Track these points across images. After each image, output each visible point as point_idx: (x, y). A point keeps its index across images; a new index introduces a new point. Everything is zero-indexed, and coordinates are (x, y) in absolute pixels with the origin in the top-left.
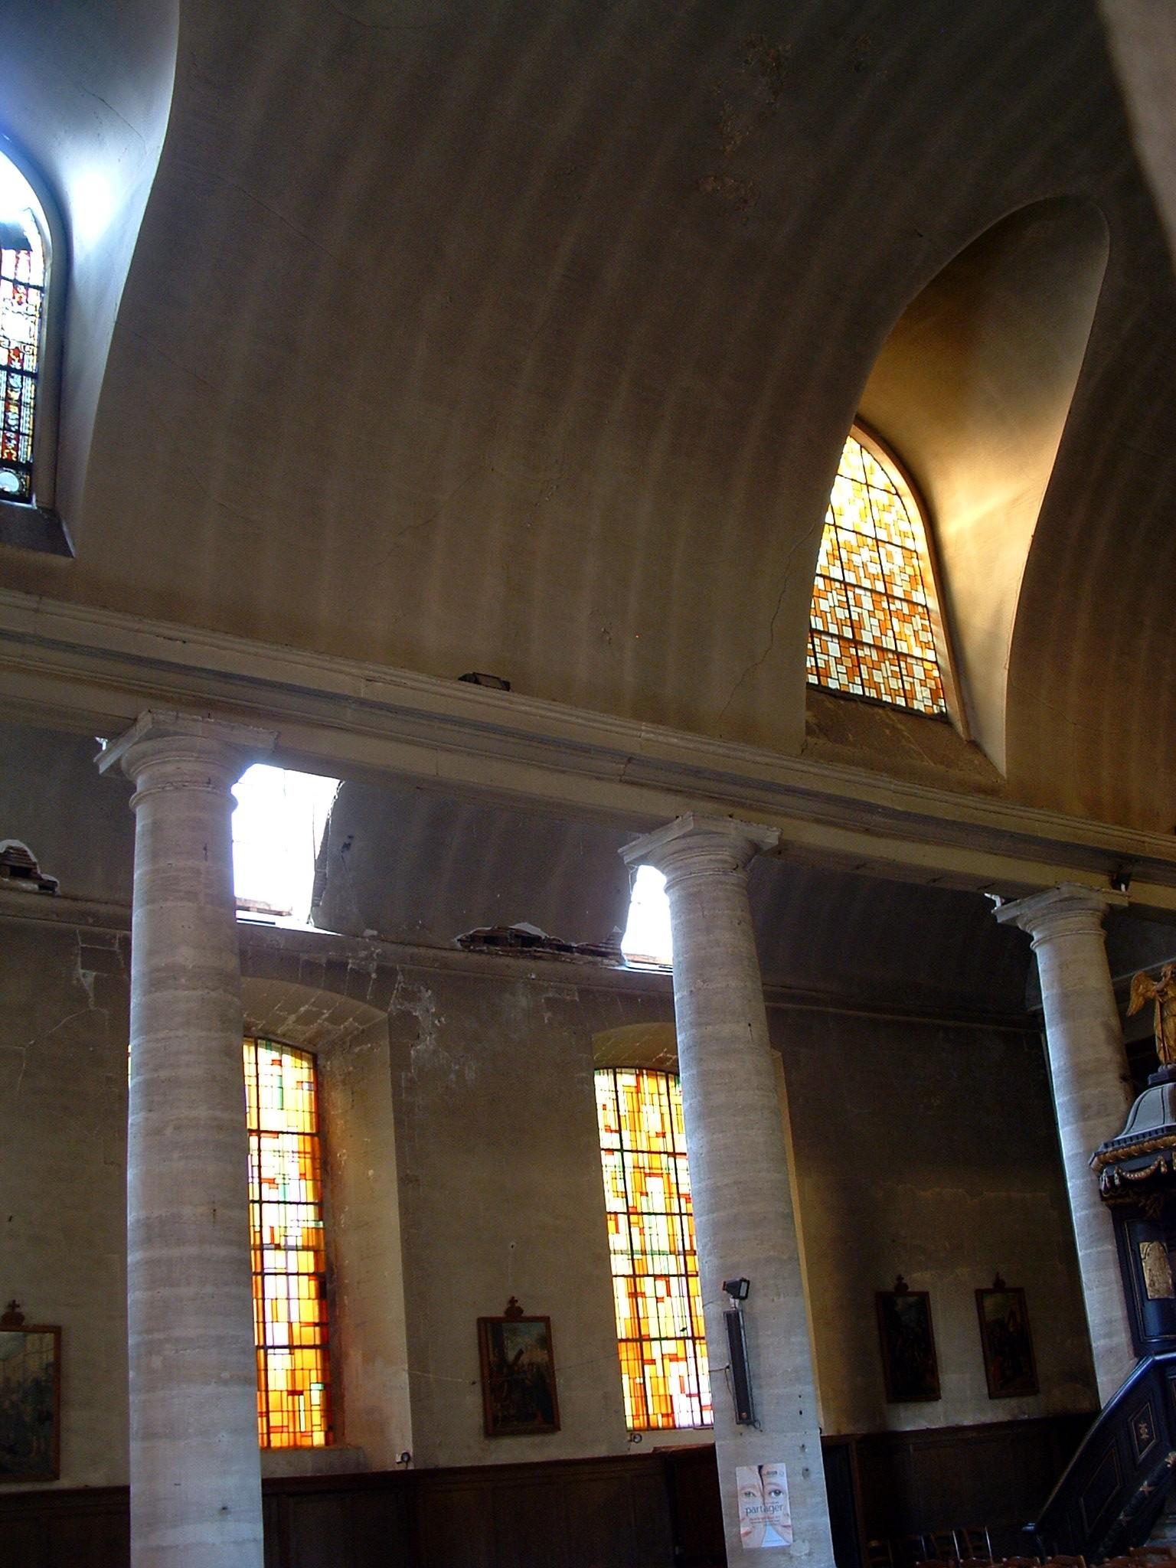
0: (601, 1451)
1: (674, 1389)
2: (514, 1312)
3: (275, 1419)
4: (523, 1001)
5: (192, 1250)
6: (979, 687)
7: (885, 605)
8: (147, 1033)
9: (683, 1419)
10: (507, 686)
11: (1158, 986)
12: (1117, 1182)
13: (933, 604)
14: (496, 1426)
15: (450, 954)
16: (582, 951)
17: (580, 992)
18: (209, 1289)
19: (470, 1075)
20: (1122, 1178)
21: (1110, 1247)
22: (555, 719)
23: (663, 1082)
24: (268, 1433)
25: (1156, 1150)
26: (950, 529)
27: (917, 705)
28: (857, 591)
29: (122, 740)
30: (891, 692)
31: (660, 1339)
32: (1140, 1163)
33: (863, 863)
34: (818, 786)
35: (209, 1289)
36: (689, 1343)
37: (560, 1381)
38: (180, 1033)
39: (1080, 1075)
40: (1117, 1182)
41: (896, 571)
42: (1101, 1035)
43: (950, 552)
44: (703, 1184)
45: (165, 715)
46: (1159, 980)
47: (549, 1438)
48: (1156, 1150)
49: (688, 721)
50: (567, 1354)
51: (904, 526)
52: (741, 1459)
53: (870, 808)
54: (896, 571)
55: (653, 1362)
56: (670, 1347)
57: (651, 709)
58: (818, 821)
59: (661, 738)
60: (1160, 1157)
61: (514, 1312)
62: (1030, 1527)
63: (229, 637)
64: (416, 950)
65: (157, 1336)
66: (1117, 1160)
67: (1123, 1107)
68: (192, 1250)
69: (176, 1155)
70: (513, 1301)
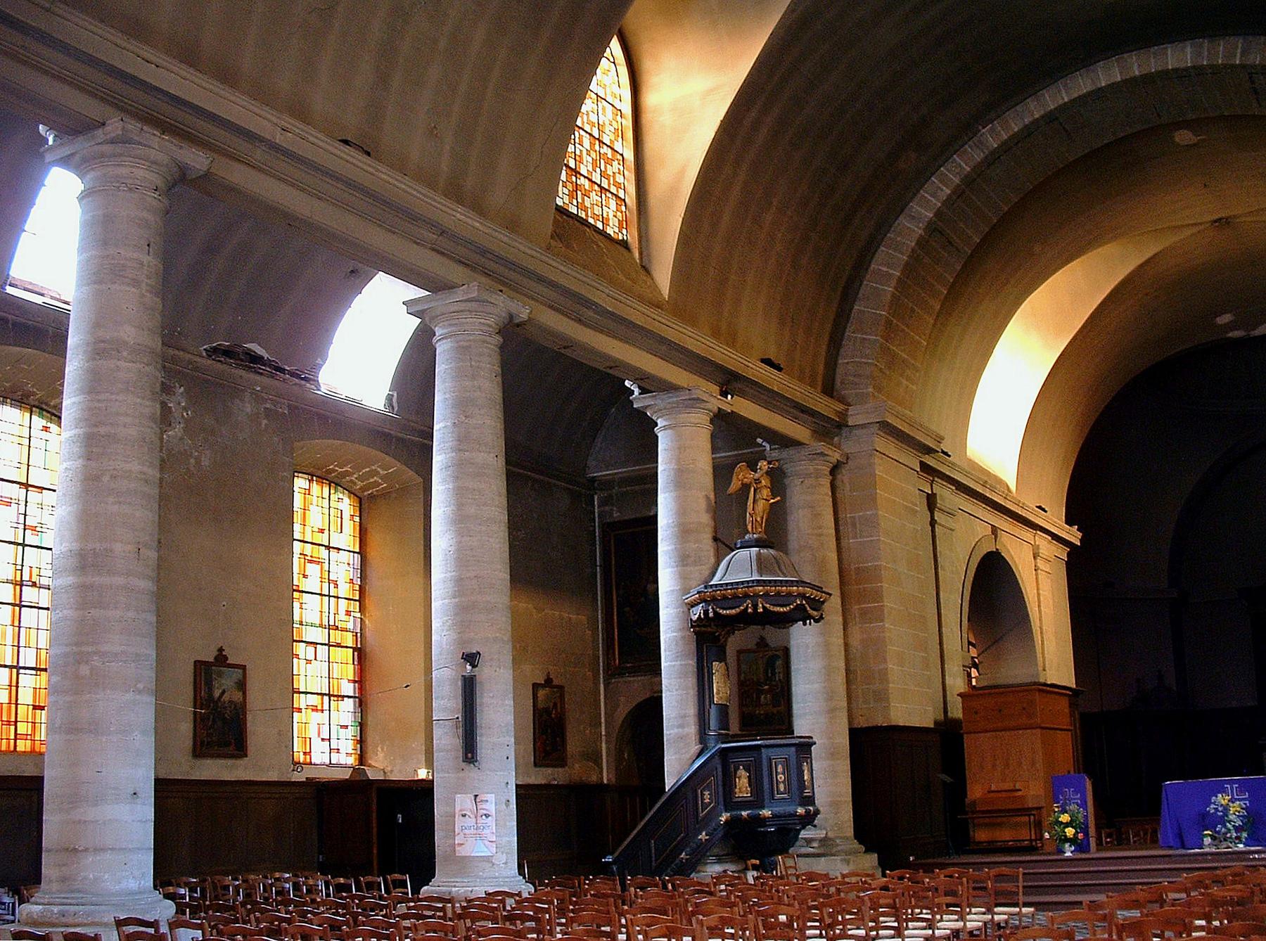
0: (273, 776)
1: (312, 732)
2: (221, 659)
3: (22, 728)
4: (248, 408)
5: (119, 580)
6: (655, 225)
7: (597, 147)
8: (90, 393)
9: (317, 758)
10: (369, 154)
11: (752, 475)
12: (711, 615)
13: (629, 155)
14: (201, 749)
15: (199, 359)
16: (292, 374)
17: (289, 406)
18: (131, 614)
19: (205, 462)
20: (715, 612)
21: (692, 662)
22: (403, 190)
23: (326, 489)
24: (15, 739)
26: (651, 99)
27: (609, 231)
29: (81, 138)
30: (595, 216)
31: (306, 693)
32: (731, 603)
33: (570, 344)
34: (562, 281)
35: (131, 614)
36: (326, 698)
37: (249, 717)
38: (120, 398)
39: (684, 532)
40: (711, 615)
41: (607, 123)
42: (703, 505)
43: (646, 118)
44: (449, 575)
45: (133, 126)
47: (239, 762)
48: (746, 596)
49: (478, 208)
50: (256, 698)
52: (460, 788)
53: (587, 303)
54: (607, 123)
55: (299, 710)
56: (315, 700)
57: (455, 192)
58: (551, 307)
59: (469, 221)
61: (221, 659)
62: (609, 859)
63: (183, 66)
64: (177, 352)
65: (85, 649)
66: (714, 599)
67: (713, 560)
68: (119, 580)
69: (111, 499)
70: (221, 650)
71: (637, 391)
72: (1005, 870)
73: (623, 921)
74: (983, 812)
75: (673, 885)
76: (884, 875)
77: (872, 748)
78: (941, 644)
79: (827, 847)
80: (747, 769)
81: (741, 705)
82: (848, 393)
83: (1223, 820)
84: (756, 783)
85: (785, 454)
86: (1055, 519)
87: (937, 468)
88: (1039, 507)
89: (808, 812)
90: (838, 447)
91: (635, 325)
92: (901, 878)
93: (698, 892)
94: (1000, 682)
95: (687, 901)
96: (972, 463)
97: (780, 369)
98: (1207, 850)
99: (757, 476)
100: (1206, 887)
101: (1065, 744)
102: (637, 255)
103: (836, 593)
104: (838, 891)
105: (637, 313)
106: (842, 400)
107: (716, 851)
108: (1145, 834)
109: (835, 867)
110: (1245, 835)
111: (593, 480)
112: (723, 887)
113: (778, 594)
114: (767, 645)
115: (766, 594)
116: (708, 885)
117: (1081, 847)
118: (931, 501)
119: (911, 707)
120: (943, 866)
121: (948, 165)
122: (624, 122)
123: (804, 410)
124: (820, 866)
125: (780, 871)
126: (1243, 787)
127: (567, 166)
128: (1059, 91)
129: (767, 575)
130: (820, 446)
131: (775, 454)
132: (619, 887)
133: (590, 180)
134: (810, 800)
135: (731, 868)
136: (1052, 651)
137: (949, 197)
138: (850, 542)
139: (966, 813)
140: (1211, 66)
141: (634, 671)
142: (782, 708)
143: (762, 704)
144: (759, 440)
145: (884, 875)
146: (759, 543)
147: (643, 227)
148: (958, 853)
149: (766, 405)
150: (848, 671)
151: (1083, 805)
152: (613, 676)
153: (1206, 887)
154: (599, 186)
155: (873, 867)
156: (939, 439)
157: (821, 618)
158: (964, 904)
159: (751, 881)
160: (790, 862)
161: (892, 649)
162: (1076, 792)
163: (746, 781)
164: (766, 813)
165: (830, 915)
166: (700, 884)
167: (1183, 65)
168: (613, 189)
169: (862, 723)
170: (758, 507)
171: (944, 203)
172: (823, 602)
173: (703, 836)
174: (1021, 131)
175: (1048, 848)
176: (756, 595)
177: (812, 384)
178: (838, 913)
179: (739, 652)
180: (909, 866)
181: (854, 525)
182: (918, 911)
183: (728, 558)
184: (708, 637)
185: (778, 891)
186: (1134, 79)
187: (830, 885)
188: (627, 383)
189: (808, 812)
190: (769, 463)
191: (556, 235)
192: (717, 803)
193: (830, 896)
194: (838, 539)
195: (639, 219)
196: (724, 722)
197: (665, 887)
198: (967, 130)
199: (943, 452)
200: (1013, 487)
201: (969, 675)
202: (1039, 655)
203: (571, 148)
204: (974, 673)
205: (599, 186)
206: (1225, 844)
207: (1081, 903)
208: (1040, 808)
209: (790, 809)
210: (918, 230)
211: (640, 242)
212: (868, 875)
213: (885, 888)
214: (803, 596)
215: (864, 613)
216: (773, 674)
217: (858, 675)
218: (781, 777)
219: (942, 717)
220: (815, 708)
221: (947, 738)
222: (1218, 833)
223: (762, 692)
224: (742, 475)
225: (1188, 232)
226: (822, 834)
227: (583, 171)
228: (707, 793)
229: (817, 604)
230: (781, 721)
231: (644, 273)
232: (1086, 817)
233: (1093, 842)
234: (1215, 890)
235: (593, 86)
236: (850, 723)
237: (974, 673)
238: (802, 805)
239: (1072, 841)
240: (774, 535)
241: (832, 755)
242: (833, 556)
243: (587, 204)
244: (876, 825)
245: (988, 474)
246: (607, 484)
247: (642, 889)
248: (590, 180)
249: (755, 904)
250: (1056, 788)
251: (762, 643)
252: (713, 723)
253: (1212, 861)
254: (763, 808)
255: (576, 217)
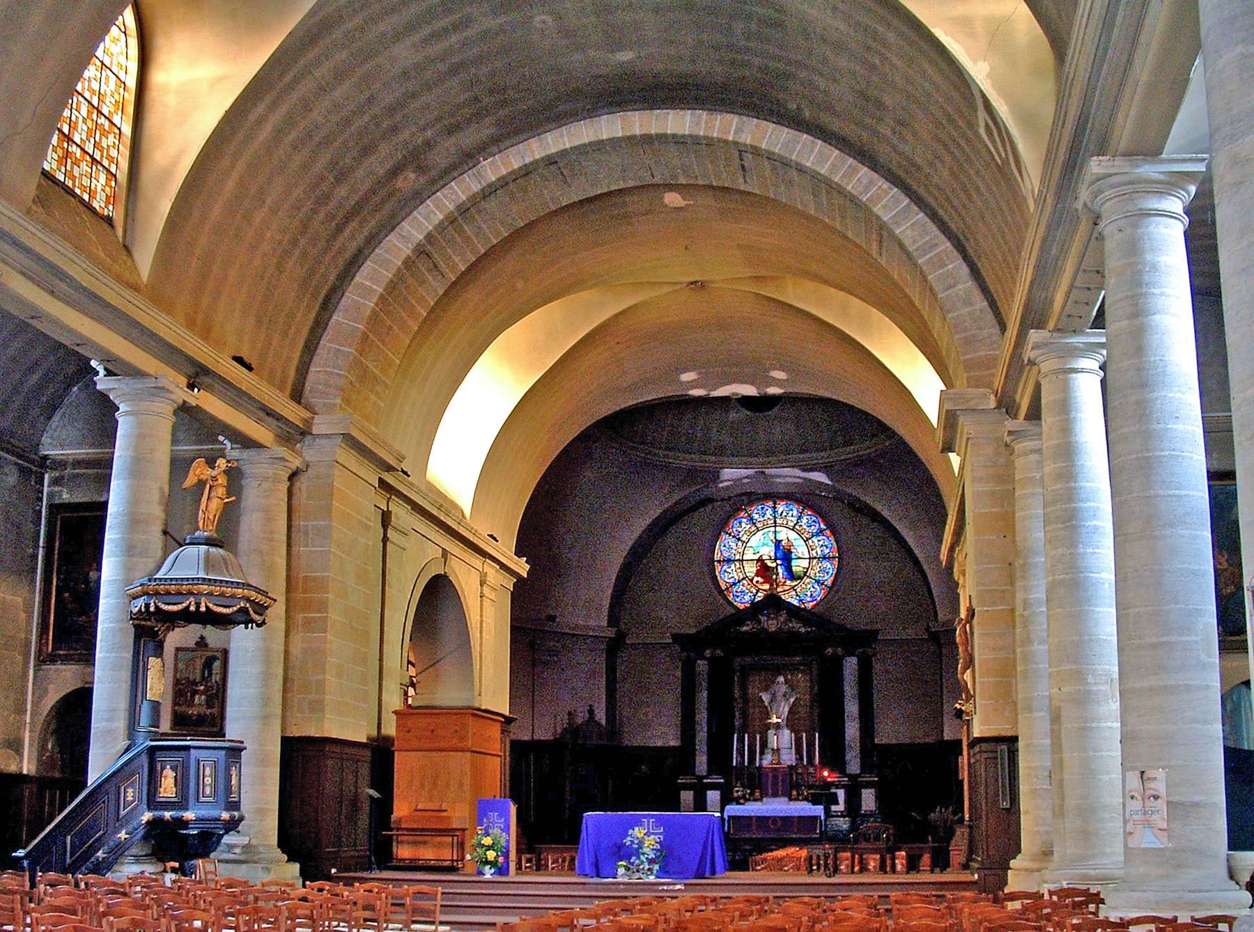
7: (95, 117)
11: (210, 472)
12: (152, 609)
13: (127, 130)
20: (157, 607)
25: (191, 593)
26: (159, 77)
27: (95, 205)
28: (80, 98)
32: (173, 599)
33: (38, 315)
34: (38, 249)
39: (134, 521)
40: (152, 609)
41: (109, 93)
43: (153, 94)
46: (213, 468)
51: (122, 59)
54: (109, 93)
60: (192, 599)
62: (21, 853)
67: (159, 553)
71: (102, 372)
72: (424, 888)
73: (28, 920)
74: (407, 829)
75: (86, 884)
76: (304, 886)
77: (300, 757)
78: (381, 660)
79: (249, 855)
80: (174, 769)
81: (175, 704)
82: (316, 401)
83: (637, 853)
84: (182, 783)
85: (246, 454)
86: (505, 549)
87: (397, 486)
88: (491, 536)
89: (232, 817)
90: (300, 454)
91: (109, 305)
92: (320, 890)
93: (114, 892)
94: (438, 703)
95: (99, 901)
96: (431, 486)
97: (250, 368)
98: (619, 880)
99: (214, 473)
100: (615, 915)
101: (496, 768)
102: (120, 233)
103: (281, 599)
104: (257, 899)
105: (112, 293)
106: (308, 407)
107: (134, 851)
108: (564, 861)
109: (256, 875)
110: (656, 867)
111: (45, 458)
112: (138, 888)
113: (222, 595)
114: (206, 645)
115: (210, 594)
116: (122, 885)
117: (502, 870)
118: (386, 518)
119: (348, 724)
120: (363, 880)
121: (445, 191)
122: (126, 95)
123: (270, 413)
124: (240, 873)
125: (200, 875)
126: (659, 822)
127: (60, 131)
128: (562, 136)
129: (214, 574)
130: (282, 451)
131: (235, 454)
132: (28, 884)
133: (83, 149)
134: (235, 806)
135: (150, 869)
136: (490, 681)
137: (442, 222)
138: (300, 549)
139: (391, 830)
140: (706, 138)
141: (66, 659)
142: (215, 711)
143: (199, 707)
144: (221, 438)
145: (304, 886)
146: (209, 542)
147: (130, 207)
148: (380, 869)
149: (235, 405)
150: (286, 680)
151: (506, 829)
152: (44, 662)
153: (615, 915)
154: (92, 157)
155: (293, 878)
156: (401, 459)
157: (264, 623)
158: (382, 919)
159: (168, 884)
160: (210, 867)
161: (332, 660)
162: (500, 816)
163: (172, 781)
164: (189, 815)
165: (246, 923)
166: (115, 884)
167: (680, 132)
168: (105, 163)
169: (295, 732)
170: (212, 506)
171: (436, 228)
172: (267, 608)
173: (123, 835)
174: (520, 168)
175: (470, 868)
176: (200, 594)
177: (281, 388)
178: (254, 921)
179: (178, 649)
180: (329, 878)
181: (306, 534)
182: (335, 923)
183: (176, 553)
184: (147, 631)
185: (195, 896)
186: (634, 137)
187: (248, 893)
188: (93, 363)
189: (232, 817)
190: (228, 461)
191: (38, 200)
192: (140, 800)
193: (247, 904)
194: (289, 545)
195: (128, 196)
196: (155, 722)
197: (77, 885)
198: (468, 158)
199: (403, 471)
200: (467, 513)
201: (406, 694)
202: (477, 680)
203: (66, 113)
204: (411, 691)
205: (92, 157)
206: (637, 875)
207: (494, 924)
208: (464, 830)
209: (214, 813)
210: (407, 250)
211: (125, 222)
212: (288, 885)
213: (304, 899)
214: (248, 599)
215: (308, 622)
216: (210, 674)
217: (292, 683)
218: (208, 780)
219: (375, 733)
220: (250, 714)
221: (380, 754)
222: (632, 864)
223: (195, 692)
224: (200, 470)
225: (666, 289)
226: (245, 840)
227: (77, 139)
228: (130, 790)
229: (261, 609)
230: (212, 725)
231: (125, 252)
232: (508, 841)
233: (512, 866)
234: (623, 918)
235: (99, 53)
236: (283, 729)
237: (411, 691)
238: (227, 809)
239: (493, 864)
240: (224, 538)
241: (263, 762)
242: (282, 562)
243: (76, 173)
244: (297, 840)
245: (445, 497)
246: (60, 464)
247: (52, 886)
248: (83, 149)
249: (170, 908)
250: (482, 810)
251: (202, 643)
252: (144, 719)
253: (624, 890)
254: (186, 809)
255: (62, 185)
